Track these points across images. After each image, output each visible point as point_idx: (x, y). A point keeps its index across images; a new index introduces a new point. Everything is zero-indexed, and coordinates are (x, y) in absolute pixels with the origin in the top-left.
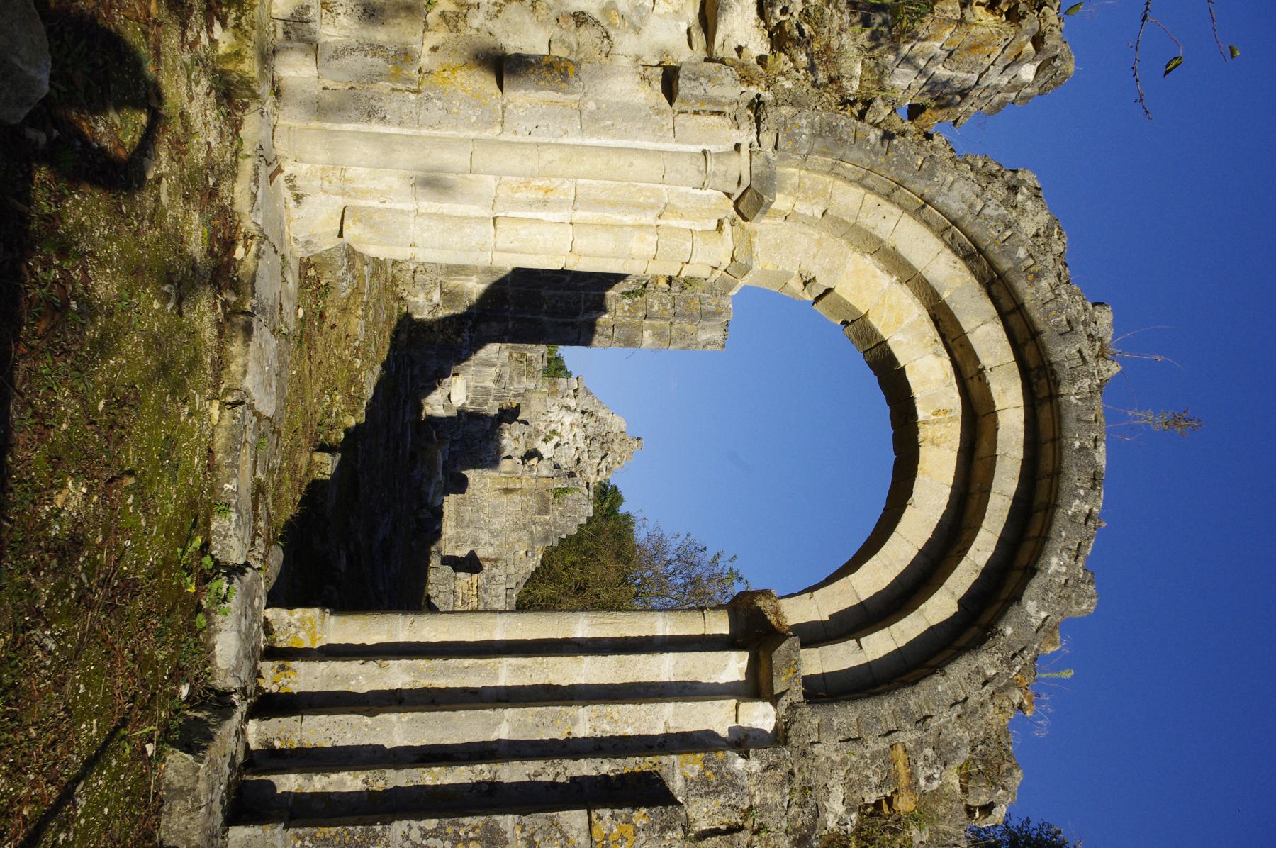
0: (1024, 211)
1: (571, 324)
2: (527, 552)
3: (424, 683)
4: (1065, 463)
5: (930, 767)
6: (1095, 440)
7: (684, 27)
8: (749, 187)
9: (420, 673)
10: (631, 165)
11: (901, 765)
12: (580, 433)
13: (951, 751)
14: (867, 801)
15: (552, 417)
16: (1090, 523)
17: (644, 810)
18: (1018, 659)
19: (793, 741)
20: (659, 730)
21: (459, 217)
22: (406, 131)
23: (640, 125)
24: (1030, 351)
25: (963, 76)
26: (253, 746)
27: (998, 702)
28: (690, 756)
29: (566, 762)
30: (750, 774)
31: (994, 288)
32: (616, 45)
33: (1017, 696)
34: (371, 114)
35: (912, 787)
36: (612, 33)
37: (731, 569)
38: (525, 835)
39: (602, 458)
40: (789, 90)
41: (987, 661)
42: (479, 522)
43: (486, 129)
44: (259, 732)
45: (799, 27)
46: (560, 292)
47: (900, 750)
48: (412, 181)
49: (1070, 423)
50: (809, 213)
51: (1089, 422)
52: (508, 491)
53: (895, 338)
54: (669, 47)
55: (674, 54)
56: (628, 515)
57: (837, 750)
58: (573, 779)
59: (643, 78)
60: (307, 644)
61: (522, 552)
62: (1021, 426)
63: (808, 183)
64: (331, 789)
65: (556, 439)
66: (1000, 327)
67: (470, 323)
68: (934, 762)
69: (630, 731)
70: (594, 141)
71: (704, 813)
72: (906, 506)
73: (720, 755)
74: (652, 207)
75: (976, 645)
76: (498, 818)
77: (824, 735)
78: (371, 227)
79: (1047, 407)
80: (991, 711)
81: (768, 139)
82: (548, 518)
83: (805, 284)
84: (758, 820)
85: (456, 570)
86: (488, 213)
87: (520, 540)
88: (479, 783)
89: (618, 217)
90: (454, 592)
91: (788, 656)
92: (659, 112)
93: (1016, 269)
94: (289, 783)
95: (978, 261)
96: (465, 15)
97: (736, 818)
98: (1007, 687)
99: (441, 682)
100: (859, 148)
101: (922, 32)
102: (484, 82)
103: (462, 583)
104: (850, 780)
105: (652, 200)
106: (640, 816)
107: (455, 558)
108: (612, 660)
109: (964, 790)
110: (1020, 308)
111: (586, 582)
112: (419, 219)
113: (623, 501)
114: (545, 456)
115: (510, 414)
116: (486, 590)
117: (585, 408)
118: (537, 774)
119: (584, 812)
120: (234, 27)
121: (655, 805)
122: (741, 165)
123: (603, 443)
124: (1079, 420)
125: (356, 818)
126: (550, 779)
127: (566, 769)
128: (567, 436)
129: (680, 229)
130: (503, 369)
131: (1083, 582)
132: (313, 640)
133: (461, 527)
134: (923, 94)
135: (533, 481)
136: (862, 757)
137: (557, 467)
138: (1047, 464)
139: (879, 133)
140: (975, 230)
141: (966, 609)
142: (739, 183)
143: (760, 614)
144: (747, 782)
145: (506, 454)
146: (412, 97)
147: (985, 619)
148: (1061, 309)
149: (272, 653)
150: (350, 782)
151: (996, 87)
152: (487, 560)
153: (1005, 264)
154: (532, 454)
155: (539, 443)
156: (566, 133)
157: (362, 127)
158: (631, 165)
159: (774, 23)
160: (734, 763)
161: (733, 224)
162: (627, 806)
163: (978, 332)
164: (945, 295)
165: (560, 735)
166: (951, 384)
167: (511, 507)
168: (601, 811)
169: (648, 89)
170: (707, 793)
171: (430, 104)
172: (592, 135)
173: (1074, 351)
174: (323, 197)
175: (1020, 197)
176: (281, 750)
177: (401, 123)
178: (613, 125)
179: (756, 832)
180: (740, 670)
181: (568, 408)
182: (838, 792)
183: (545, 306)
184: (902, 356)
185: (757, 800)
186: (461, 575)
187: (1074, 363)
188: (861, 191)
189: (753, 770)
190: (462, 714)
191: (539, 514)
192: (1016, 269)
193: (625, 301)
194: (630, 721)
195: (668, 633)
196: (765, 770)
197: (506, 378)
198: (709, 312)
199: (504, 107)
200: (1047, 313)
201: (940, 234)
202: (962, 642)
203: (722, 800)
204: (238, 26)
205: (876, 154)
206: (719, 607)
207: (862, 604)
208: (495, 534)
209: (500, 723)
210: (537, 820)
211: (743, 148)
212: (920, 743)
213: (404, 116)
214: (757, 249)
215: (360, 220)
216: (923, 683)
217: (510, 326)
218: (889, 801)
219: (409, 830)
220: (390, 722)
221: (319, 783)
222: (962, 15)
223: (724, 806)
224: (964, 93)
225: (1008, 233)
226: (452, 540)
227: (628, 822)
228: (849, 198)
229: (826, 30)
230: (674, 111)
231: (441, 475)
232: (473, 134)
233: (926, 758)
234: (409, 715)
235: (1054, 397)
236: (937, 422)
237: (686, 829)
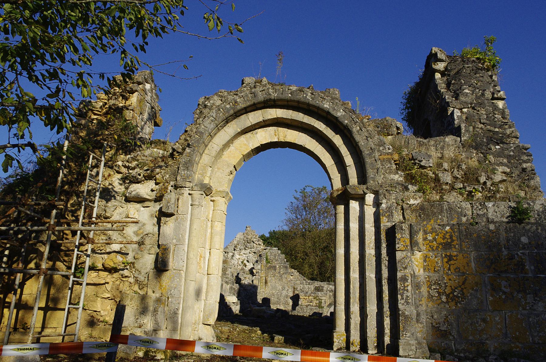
0: (213, 104)
2: (291, 275)
3: (357, 300)
4: (296, 100)
5: (386, 148)
6: (289, 89)
7: (142, 209)
8: (204, 191)
9: (355, 301)
11: (385, 157)
12: (243, 251)
13: (381, 142)
14: (395, 168)
15: (236, 263)
16: (314, 94)
17: (397, 235)
18: (354, 119)
19: (377, 189)
20: (373, 229)
21: (207, 286)
22: (182, 302)
24: (258, 106)
25: (147, 109)
26: (376, 352)
27: (367, 126)
28: (381, 220)
29: (382, 257)
30: (387, 203)
31: (238, 115)
32: (150, 232)
33: (365, 120)
34: (175, 313)
35: (391, 154)
36: (145, 233)
37: (300, 192)
38: (403, 270)
39: (254, 243)
40: (169, 176)
41: (355, 129)
42: (278, 295)
43: (182, 276)
44: (372, 350)
45: (145, 171)
47: (380, 157)
48: (196, 301)
49: (283, 97)
51: (283, 90)
52: (266, 282)
53: (251, 146)
54: (150, 214)
55: (152, 212)
56: (270, 233)
57: (380, 176)
58: (387, 255)
59: (165, 223)
60: (345, 337)
61: (291, 277)
62: (282, 110)
64: (389, 327)
65: (245, 262)
66: (250, 113)
68: (384, 147)
69: (373, 238)
70: (187, 241)
71: (398, 217)
72: (305, 147)
73: (381, 211)
74: (207, 223)
75: (350, 132)
76: (398, 277)
77: (376, 180)
78: (210, 315)
79: (277, 102)
80: (370, 128)
81: (188, 184)
82: (278, 266)
83: (231, 174)
84: (400, 201)
85: (298, 305)
86: (206, 277)
87: (286, 278)
88: (388, 283)
89: (208, 234)
90: (307, 306)
91: (352, 189)
92: (177, 219)
93: (234, 109)
94: (387, 340)
95: (229, 119)
96: (140, 282)
97: (399, 207)
98: (363, 123)
99: (357, 295)
100: (192, 155)
101: (135, 124)
102: (166, 277)
103: (303, 303)
105: (205, 223)
106: (398, 236)
107: (293, 305)
108: (351, 242)
109: (392, 135)
110: (245, 108)
111: (304, 252)
112: (208, 299)
113: (263, 235)
114: (252, 266)
115: (238, 280)
116: (307, 293)
117: (233, 249)
118: (386, 266)
119: (397, 252)
120: (155, 353)
121: (395, 231)
122: (197, 194)
123: (248, 242)
124: (282, 94)
125: (398, 320)
126: (387, 262)
128: (244, 257)
129: (213, 214)
130: (224, 281)
131: (329, 92)
132: (344, 335)
133: (280, 302)
134: (152, 122)
135: (262, 272)
136: (382, 168)
137: (257, 262)
138: (295, 104)
139: (187, 148)
140: (220, 120)
142: (202, 195)
143: (338, 196)
144: (389, 204)
145: (251, 283)
146: (170, 300)
147: (342, 128)
148: (247, 96)
149: (348, 348)
150: (387, 322)
151: (151, 97)
152: (294, 292)
153: (232, 112)
154: (251, 272)
155: (246, 269)
156: (184, 250)
157: (180, 316)
158: (195, 229)
159: (143, 178)
161: (212, 197)
162: (395, 240)
163: (251, 121)
164: (239, 130)
165: (374, 259)
166: (266, 129)
167: (272, 281)
168: (397, 247)
169: (169, 222)
170: (392, 216)
172: (185, 241)
173: (260, 93)
174: (200, 331)
175: (209, 104)
176: (377, 343)
177: (179, 303)
179: (403, 202)
180: (355, 203)
181: (233, 256)
182: (392, 176)
184: (257, 145)
185: (394, 201)
186: (300, 303)
187: (264, 93)
188: (204, 154)
190: (367, 288)
191: (276, 270)
192: (234, 109)
195: (343, 224)
196: (386, 198)
197: (227, 280)
199: (174, 270)
200: (248, 100)
201: (219, 130)
202: (349, 136)
203: (394, 211)
204: (155, 352)
205: (194, 150)
206: (336, 210)
207: (335, 163)
208: (283, 289)
210: (399, 265)
211: (190, 193)
212: (379, 151)
214: (221, 189)
216: (361, 149)
218: (395, 161)
220: (369, 310)
221: (387, 331)
222: (130, 110)
223: (396, 211)
224: (152, 108)
225: (221, 110)
226: (286, 305)
227: (400, 239)
228: (205, 159)
229: (147, 162)
231: (264, 308)
232: (183, 280)
234: (368, 304)
235: (274, 100)
236: (278, 135)
237: (402, 223)
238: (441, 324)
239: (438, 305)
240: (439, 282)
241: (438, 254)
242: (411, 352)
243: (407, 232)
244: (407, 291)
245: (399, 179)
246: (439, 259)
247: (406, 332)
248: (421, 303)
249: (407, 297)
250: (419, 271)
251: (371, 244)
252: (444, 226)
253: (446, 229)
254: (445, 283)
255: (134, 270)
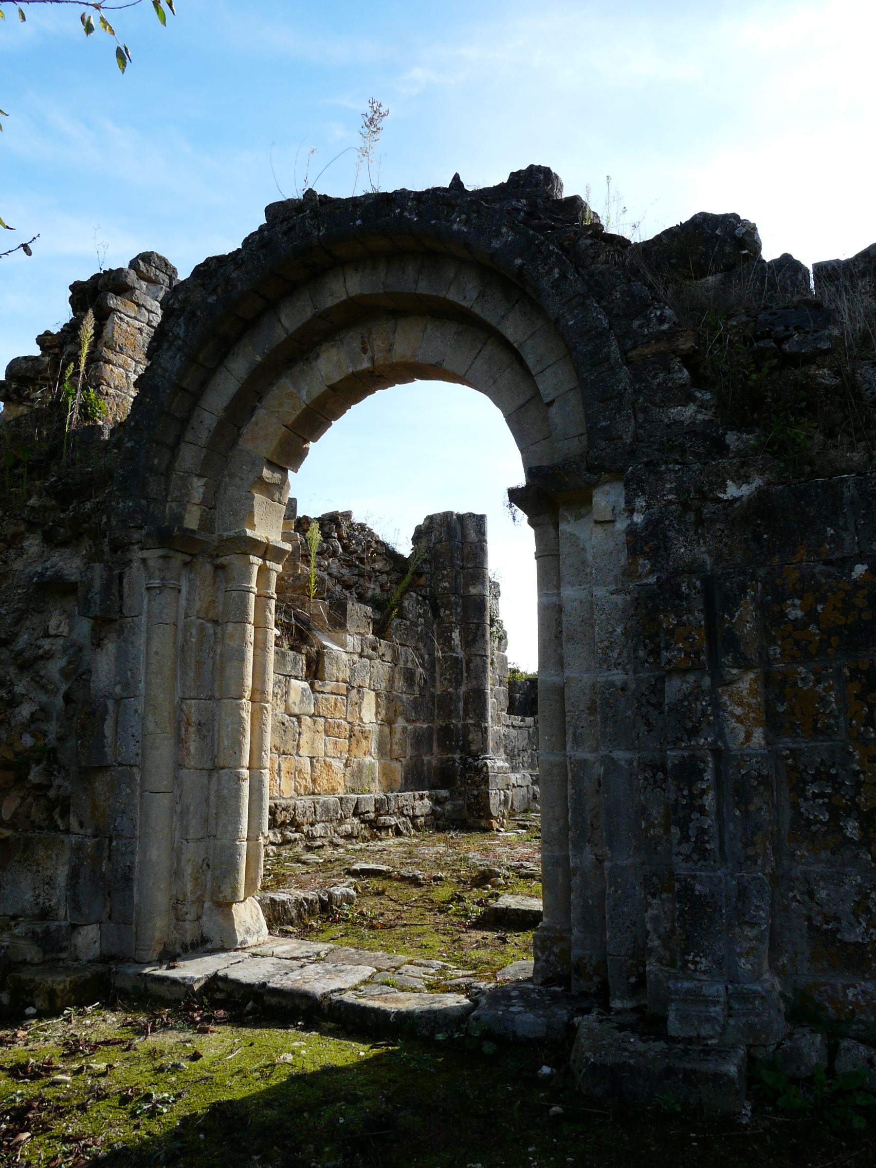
1: (468, 664)
5: (649, 320)
10: (157, 653)
11: (647, 351)
23: (130, 647)
38: (685, 737)
46: (437, 676)
50: (201, 490)
63: (177, 494)
67: (470, 760)
104: (663, 401)
127: (643, 694)
141: (517, 302)
144: (655, 510)
146: (114, 844)
160: (637, 524)
171: (119, 828)
178: (130, 670)
183: (450, 690)
189: (644, 504)
193: (442, 614)
194: (611, 630)
196: (644, 493)
198: (448, 533)
199: (120, 765)
203: (672, 534)
209: (613, 759)
213: (128, 850)
215: (219, 887)
217: (471, 721)
219: (682, 854)
230: (121, 617)
233: (641, 326)
238: (844, 923)
239: (833, 853)
240: (833, 771)
241: (826, 669)
242: (708, 1026)
243: (698, 604)
244: (702, 810)
245: (700, 417)
246: (831, 688)
247: (697, 955)
248: (751, 852)
249: (702, 831)
250: (748, 736)
251: (612, 651)
252: (846, 563)
253: (854, 575)
254: (856, 773)
255: (56, 767)
